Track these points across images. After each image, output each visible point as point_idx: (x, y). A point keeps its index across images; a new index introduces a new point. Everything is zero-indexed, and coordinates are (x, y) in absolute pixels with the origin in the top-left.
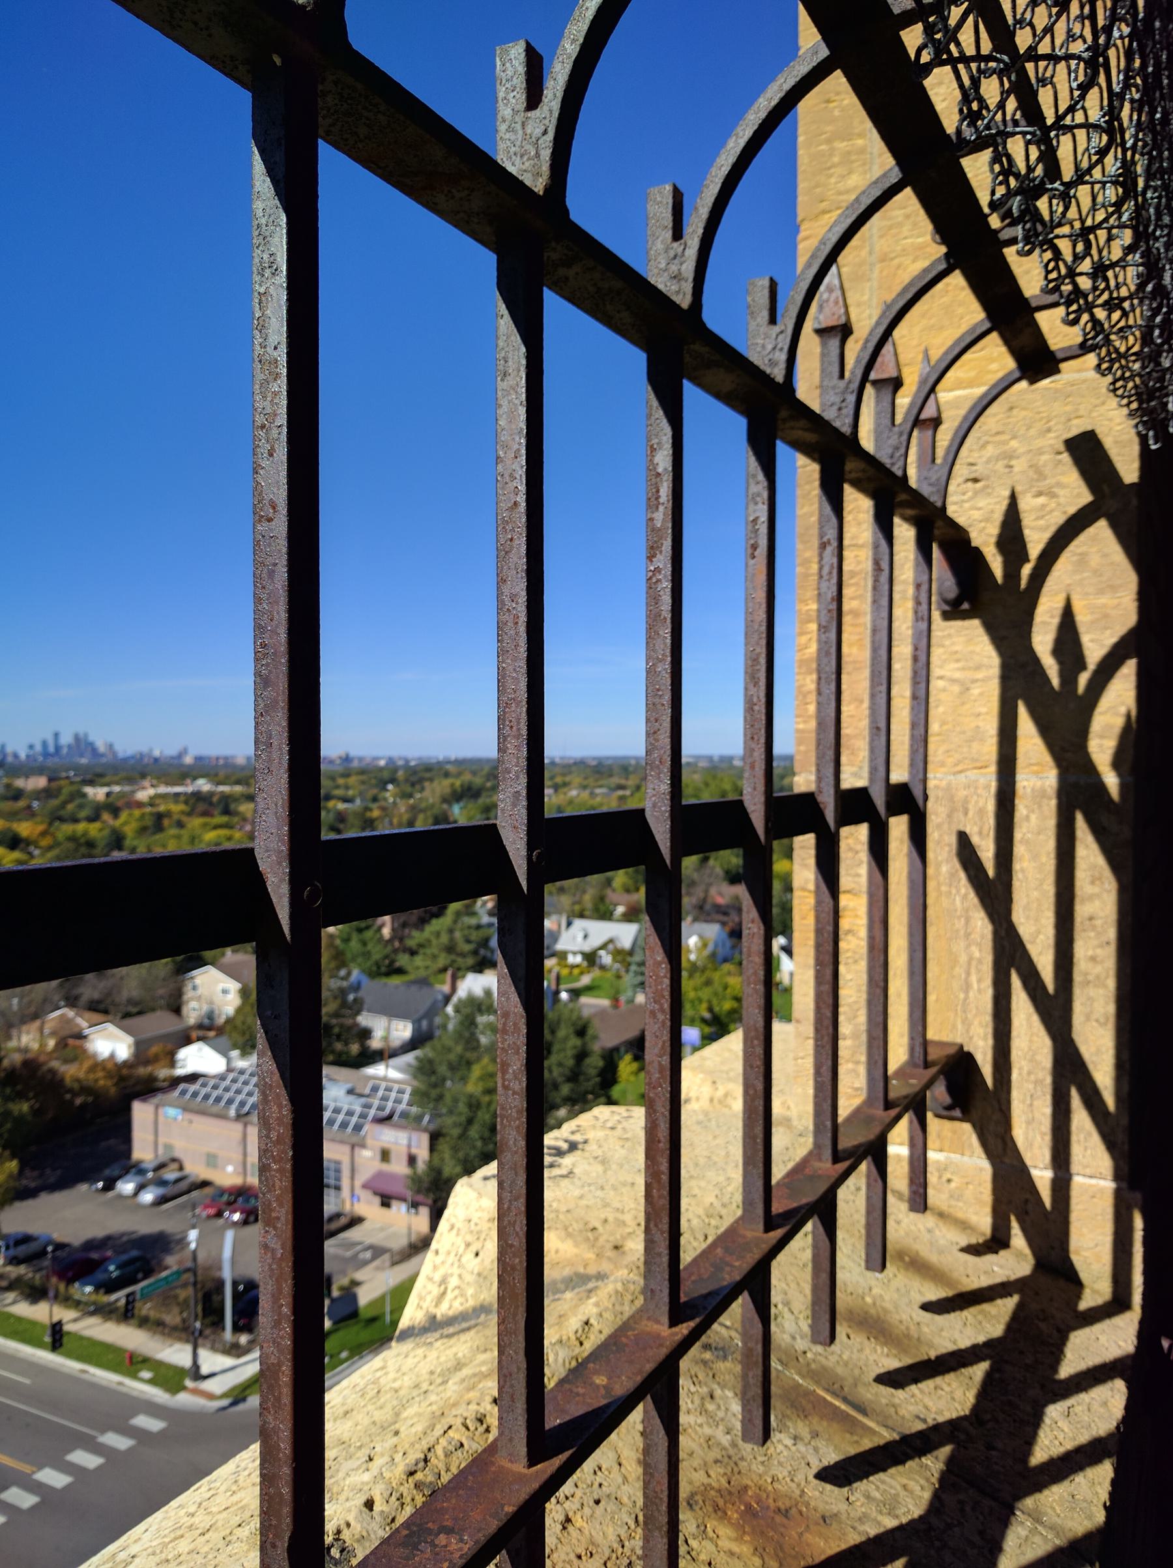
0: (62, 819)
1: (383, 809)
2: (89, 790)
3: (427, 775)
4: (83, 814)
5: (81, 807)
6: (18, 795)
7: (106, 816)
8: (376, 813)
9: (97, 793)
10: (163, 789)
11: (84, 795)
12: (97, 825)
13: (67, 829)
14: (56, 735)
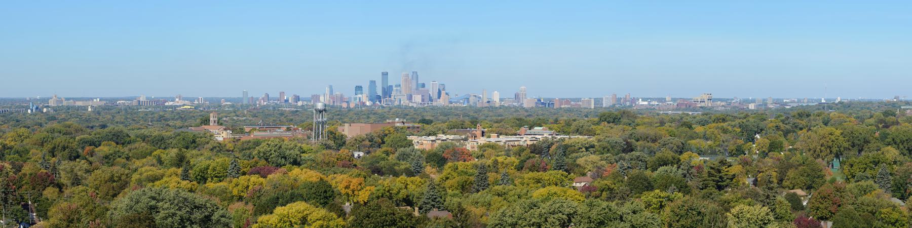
0: (379, 172)
1: (745, 163)
2: (414, 139)
3: (804, 122)
4: (404, 165)
5: (404, 157)
6: (340, 142)
7: (428, 169)
8: (736, 169)
9: (423, 143)
10: (493, 139)
11: (410, 144)
12: (417, 179)
13: (387, 181)
14: (385, 74)
